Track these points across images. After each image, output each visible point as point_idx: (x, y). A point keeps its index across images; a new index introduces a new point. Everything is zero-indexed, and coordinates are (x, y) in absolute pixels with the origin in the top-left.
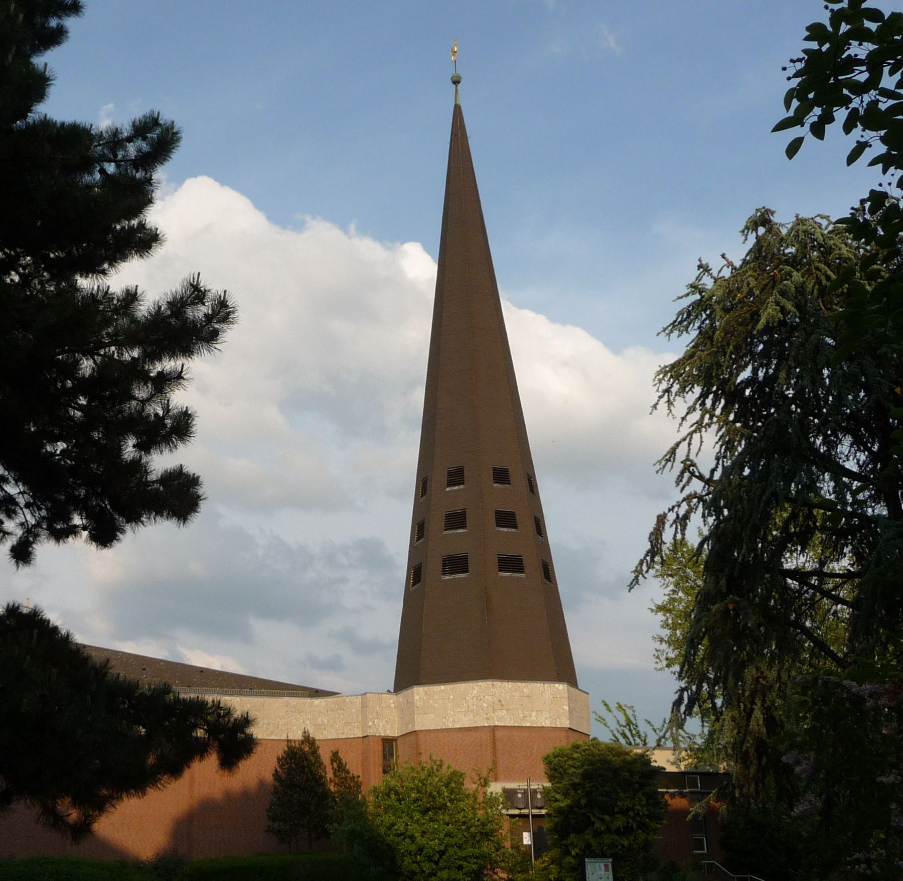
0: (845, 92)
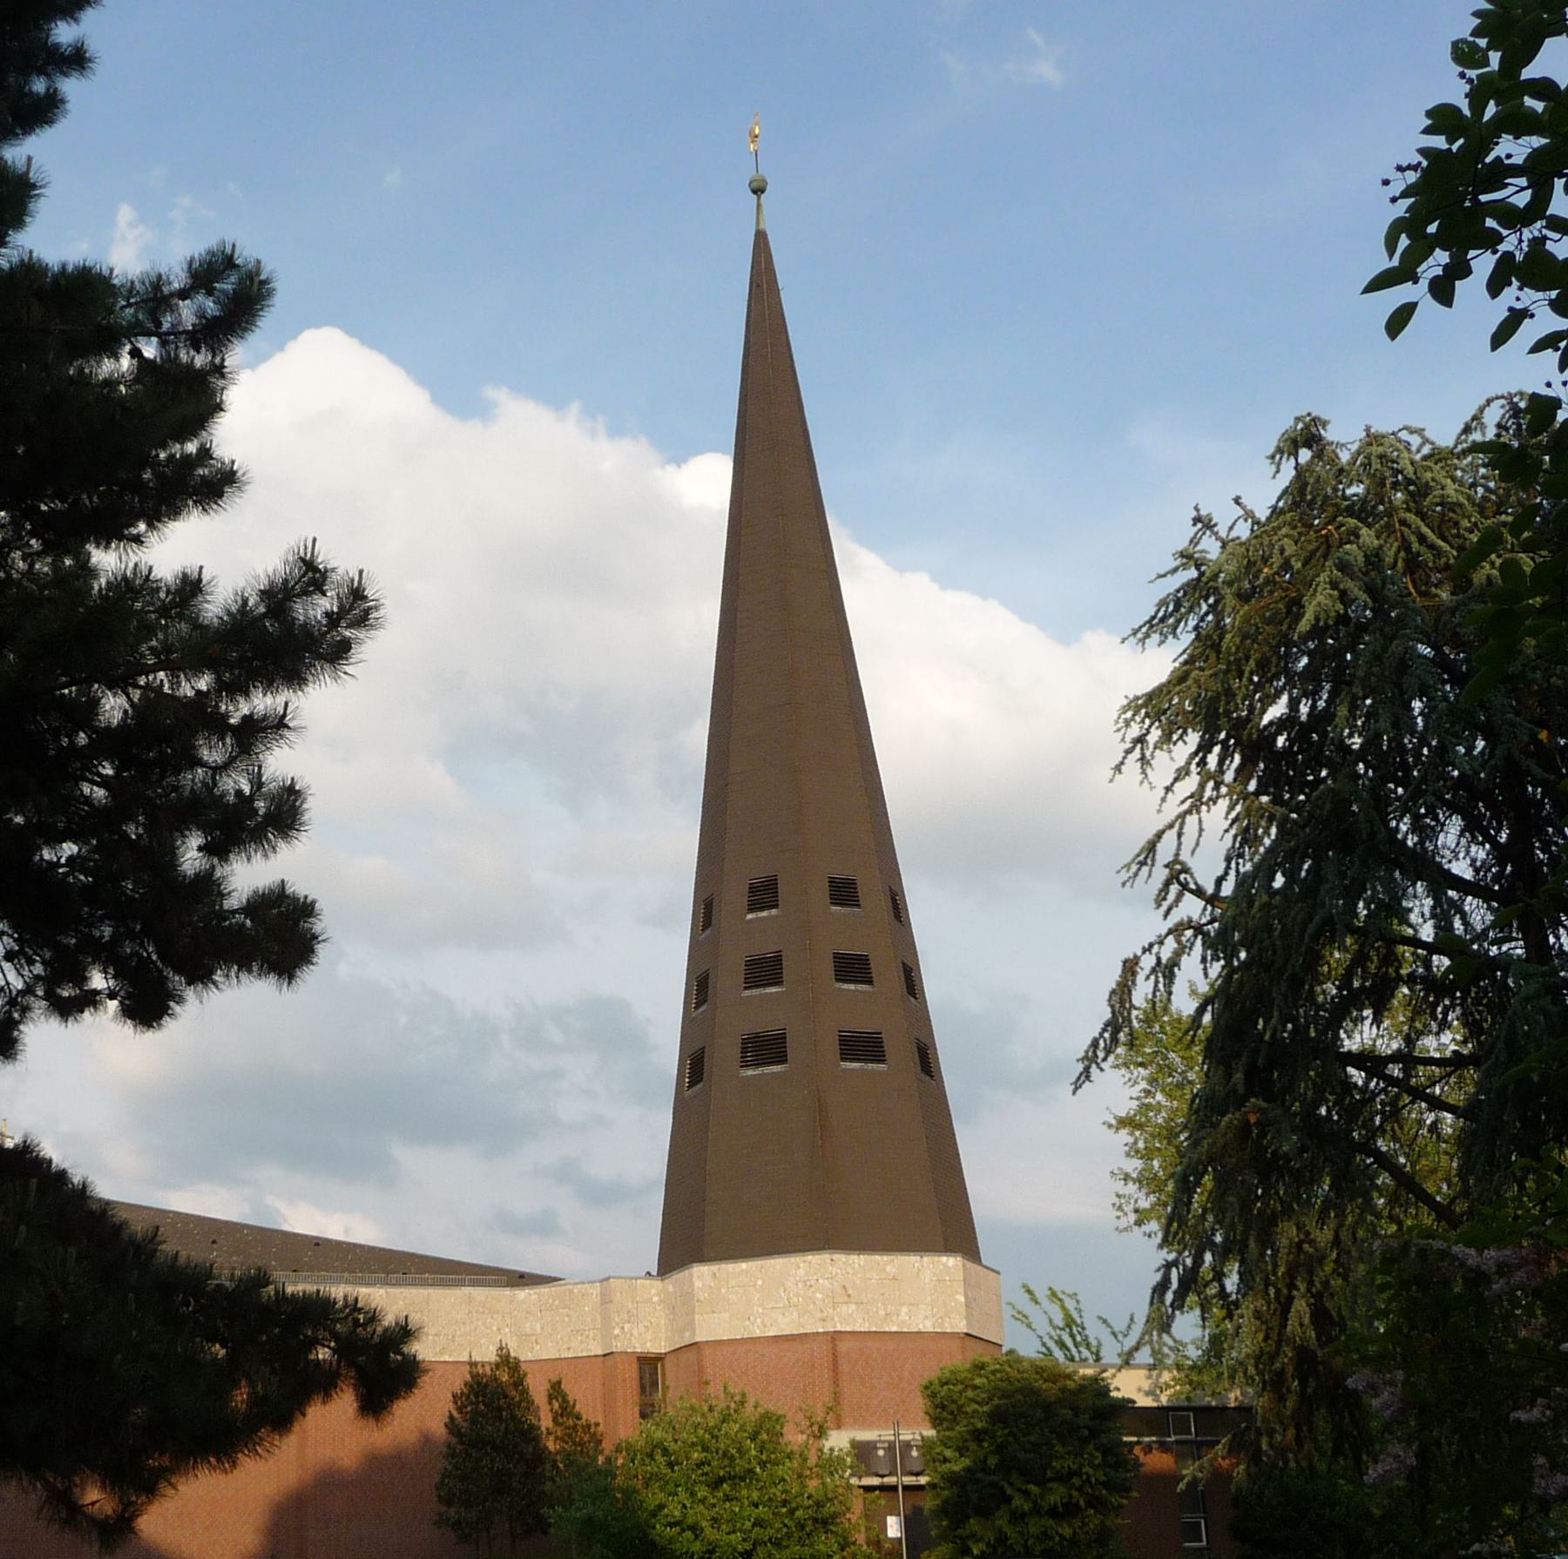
0: (1490, 223)
